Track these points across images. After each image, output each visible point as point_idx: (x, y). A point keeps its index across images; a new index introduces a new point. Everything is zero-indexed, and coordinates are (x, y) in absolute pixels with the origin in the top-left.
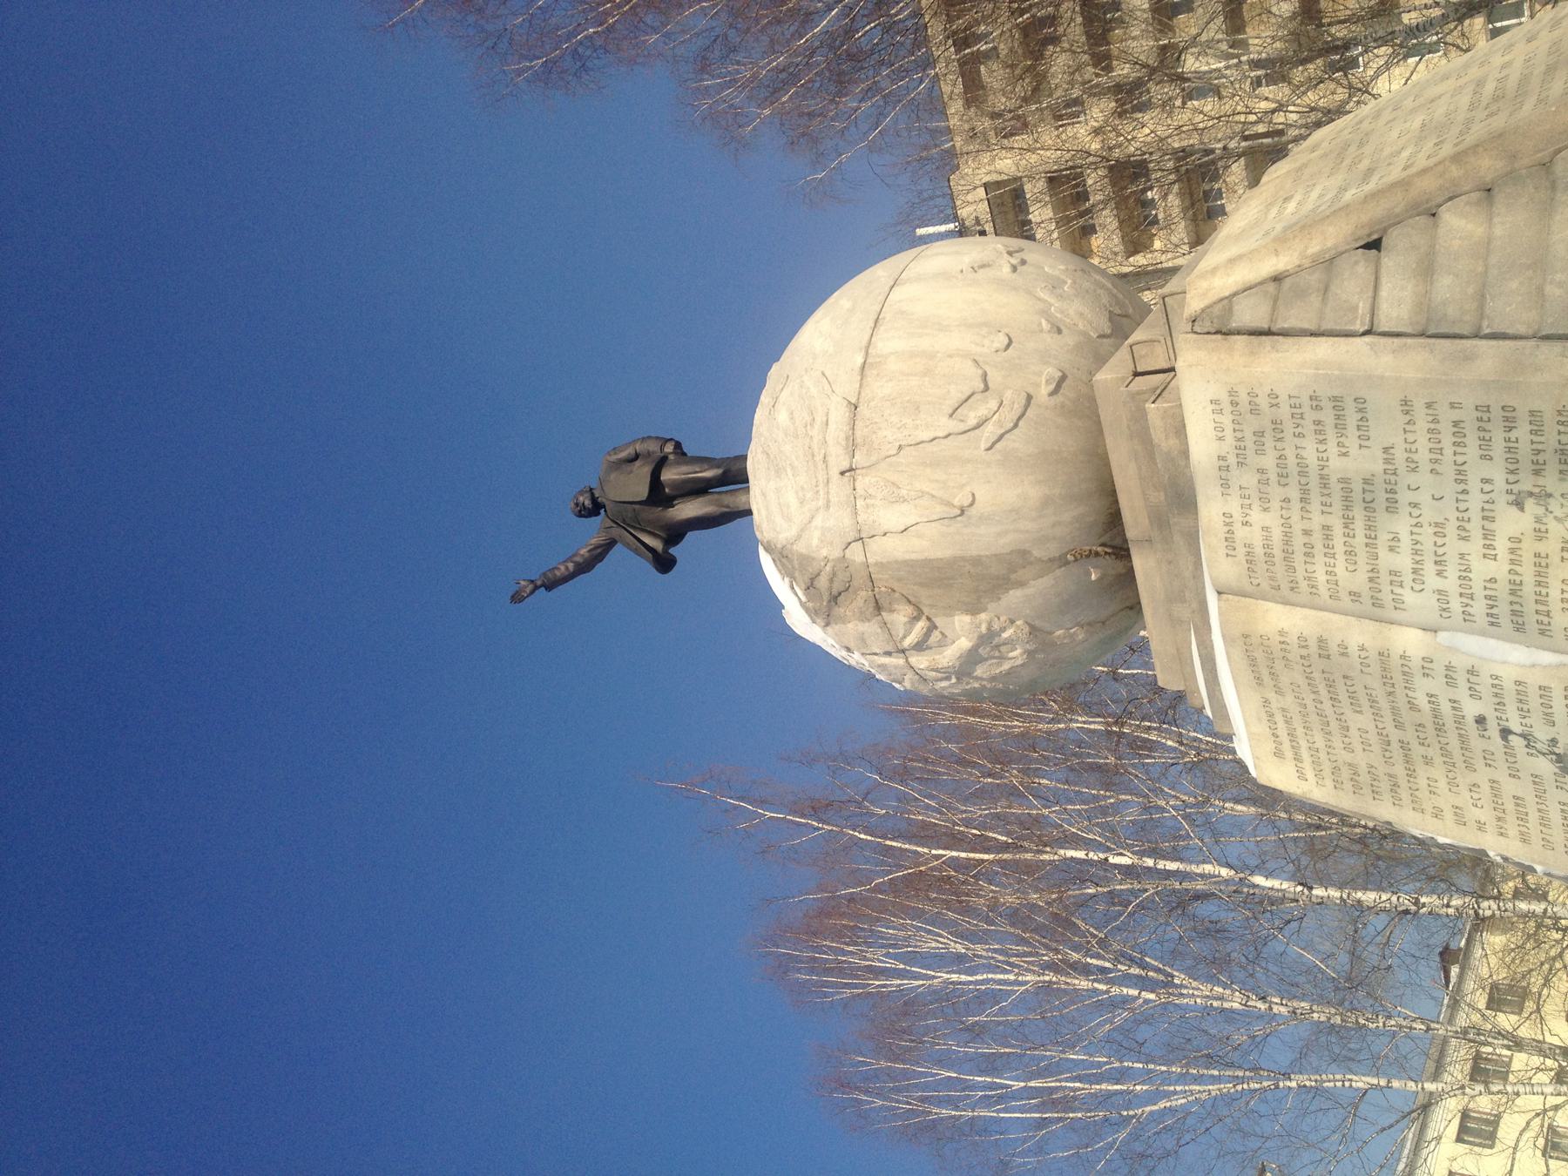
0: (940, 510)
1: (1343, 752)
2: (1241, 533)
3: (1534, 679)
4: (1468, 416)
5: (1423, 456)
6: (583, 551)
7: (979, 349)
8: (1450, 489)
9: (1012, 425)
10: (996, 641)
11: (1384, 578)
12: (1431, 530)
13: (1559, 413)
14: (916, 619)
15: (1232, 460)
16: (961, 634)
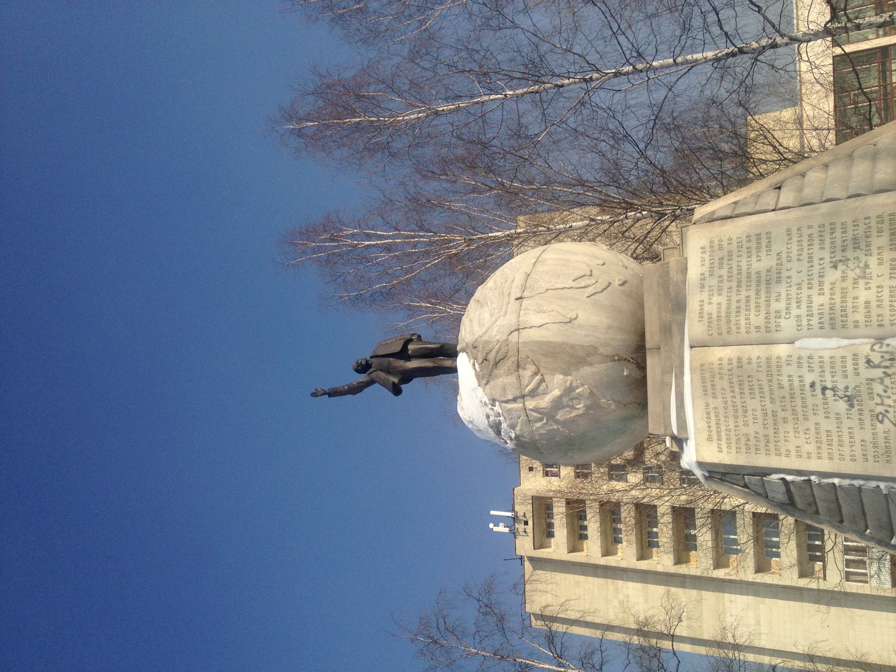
0: (560, 319)
1: (743, 427)
2: (707, 308)
3: (838, 354)
4: (815, 231)
5: (794, 255)
6: (355, 383)
7: (590, 262)
8: (805, 265)
9: (600, 290)
10: (573, 395)
11: (773, 315)
12: (796, 288)
13: (854, 221)
14: (536, 374)
15: (707, 274)
16: (556, 385)
